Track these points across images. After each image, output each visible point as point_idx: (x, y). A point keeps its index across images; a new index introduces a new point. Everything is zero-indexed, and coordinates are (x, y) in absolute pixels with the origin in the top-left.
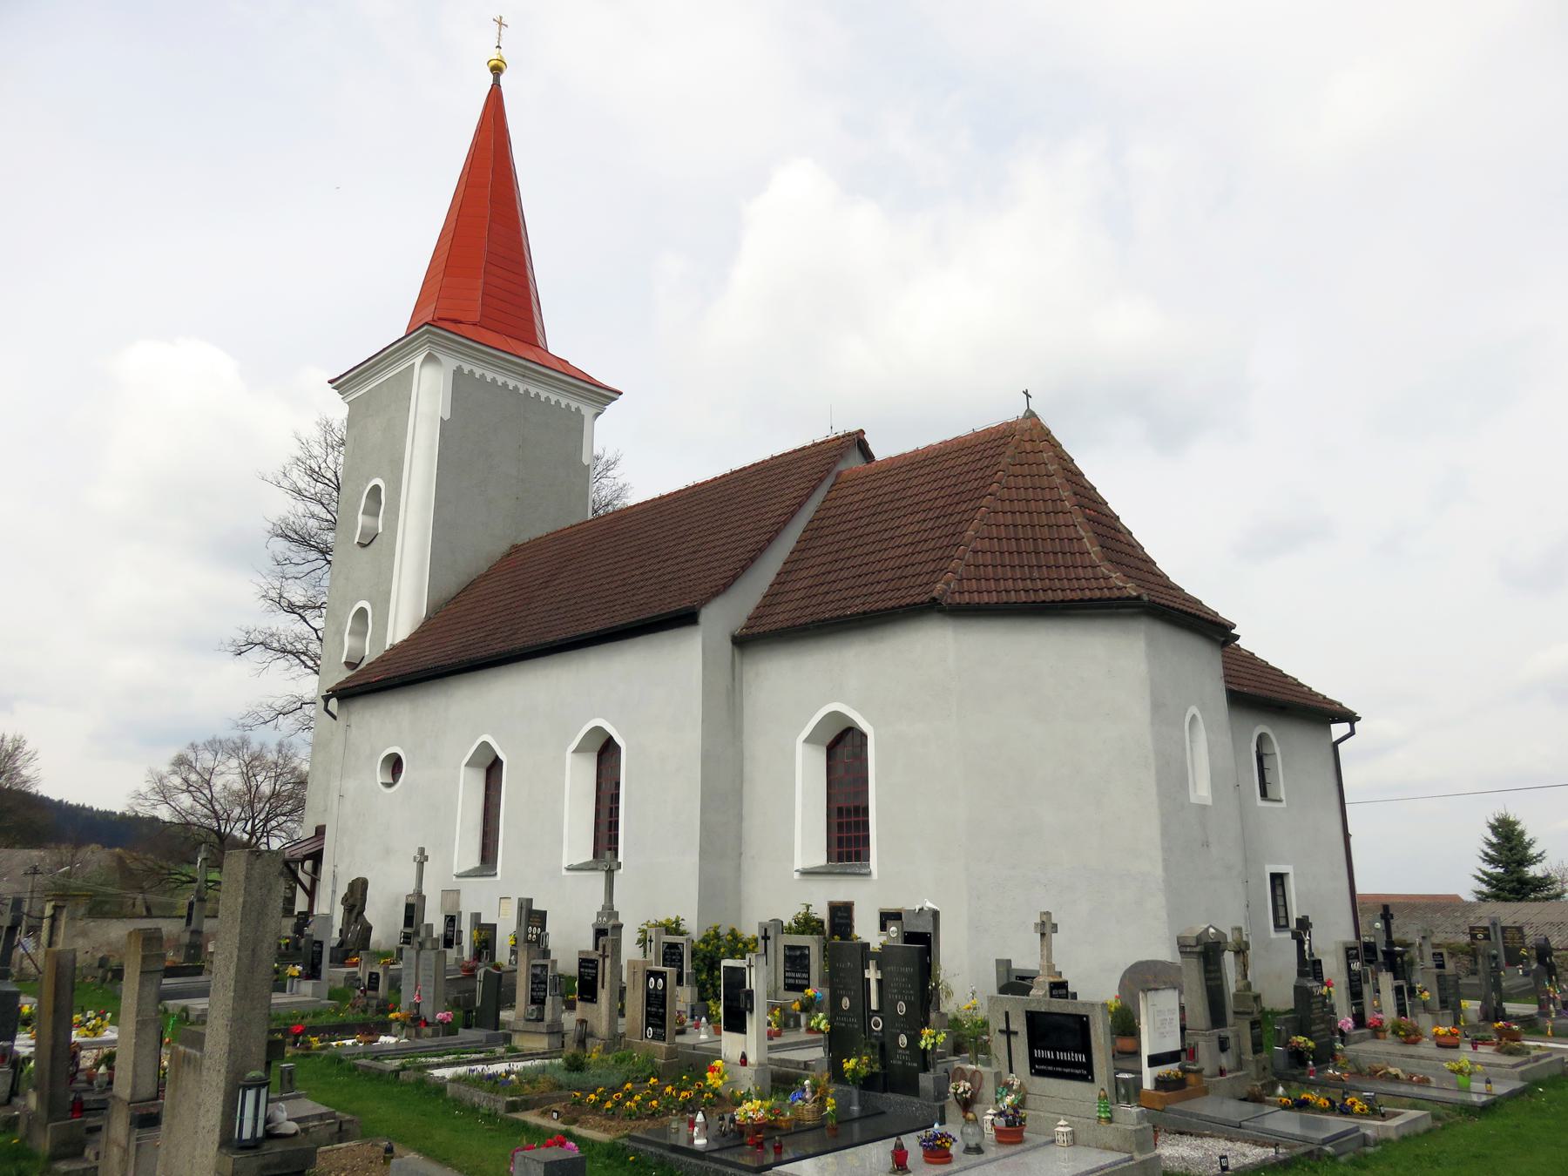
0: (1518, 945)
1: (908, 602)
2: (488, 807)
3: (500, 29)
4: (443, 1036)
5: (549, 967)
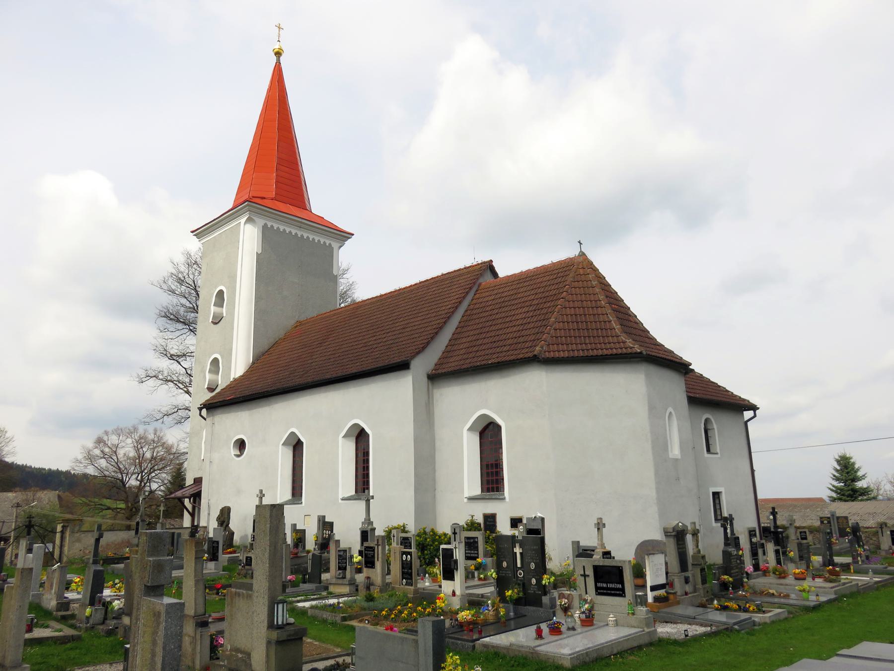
0: (845, 526)
1: (521, 357)
2: (295, 467)
3: (279, 31)
4: (291, 587)
5: (348, 551)
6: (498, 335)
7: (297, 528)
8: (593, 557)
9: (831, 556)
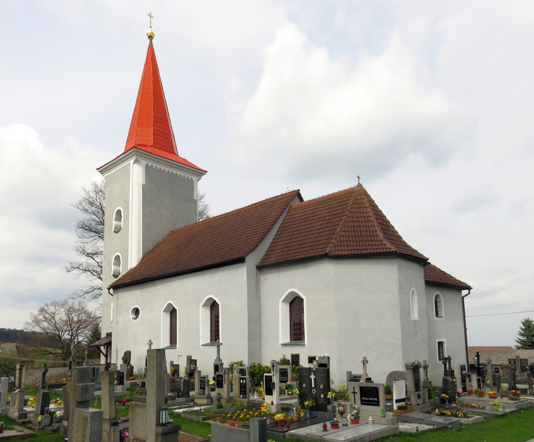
1: (317, 254)
3: (151, 19)
4: (170, 400)
6: (302, 240)
7: (174, 364)
9: (515, 384)
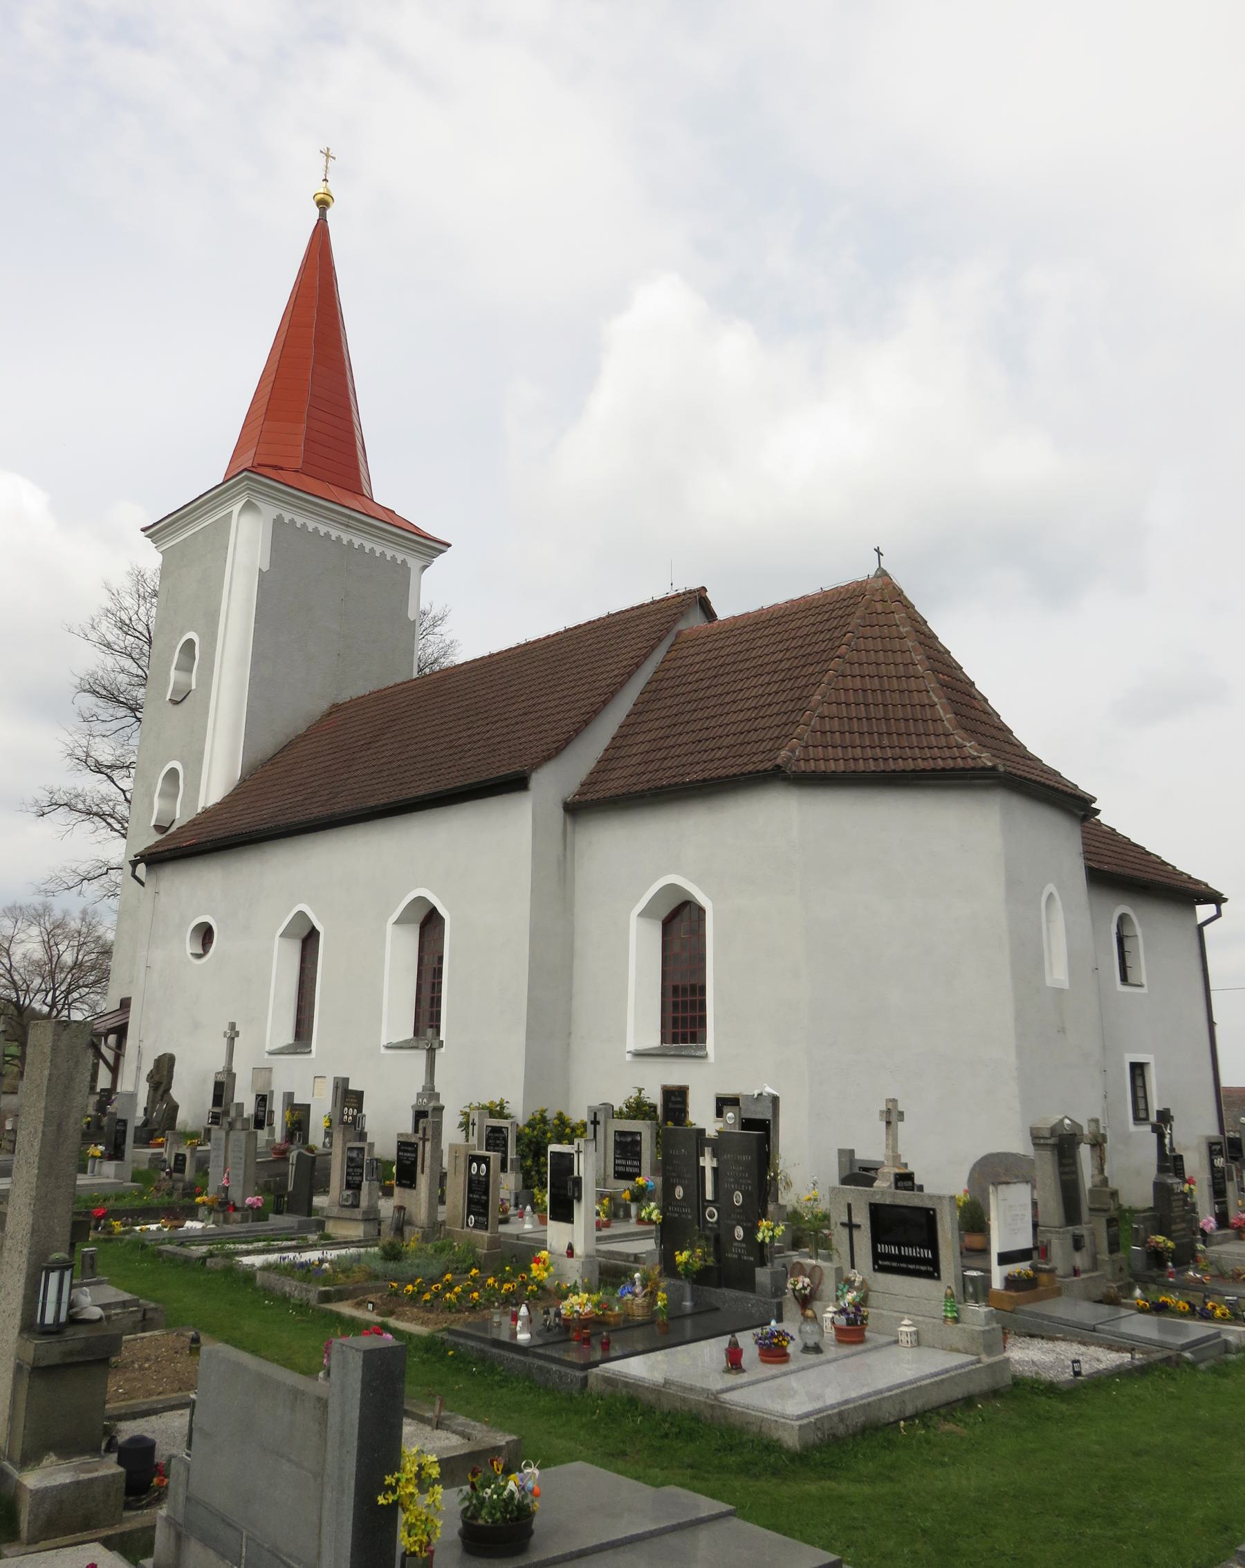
4: (252, 1221)
6: (707, 729)
7: (295, 1102)
8: (875, 1184)
